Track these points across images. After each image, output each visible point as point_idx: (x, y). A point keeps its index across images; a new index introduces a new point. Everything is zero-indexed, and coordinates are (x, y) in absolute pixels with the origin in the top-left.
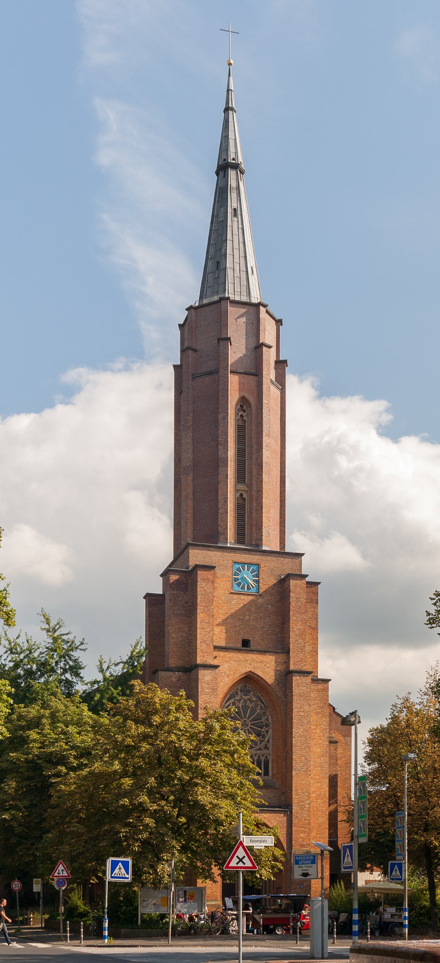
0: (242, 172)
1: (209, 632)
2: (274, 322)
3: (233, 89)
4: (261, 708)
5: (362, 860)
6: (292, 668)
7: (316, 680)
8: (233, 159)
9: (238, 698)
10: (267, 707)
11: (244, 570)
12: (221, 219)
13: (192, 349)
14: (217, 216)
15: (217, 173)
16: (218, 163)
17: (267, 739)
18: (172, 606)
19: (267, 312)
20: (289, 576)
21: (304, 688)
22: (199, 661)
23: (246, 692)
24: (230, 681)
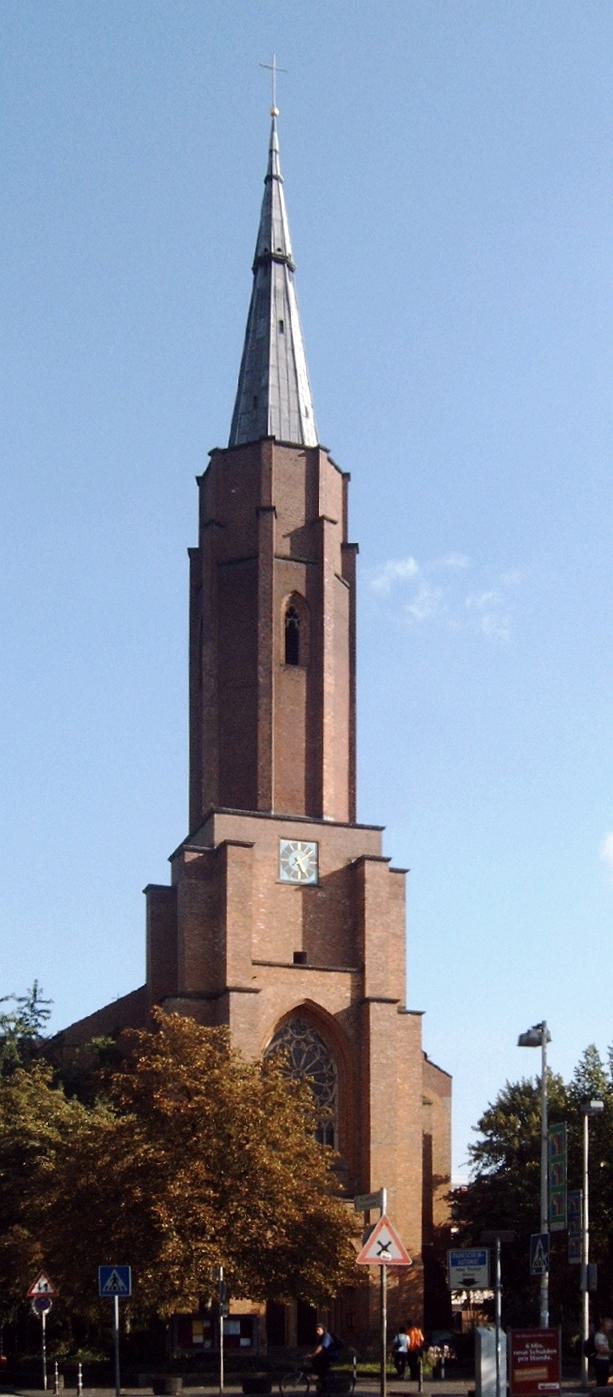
0: (291, 269)
1: (245, 940)
2: (340, 476)
3: (277, 149)
4: (322, 1053)
6: (368, 993)
7: (402, 1011)
8: (279, 250)
10: (333, 1051)
11: (296, 848)
12: (259, 336)
13: (218, 524)
14: (254, 331)
15: (255, 270)
16: (256, 255)
18: (187, 913)
19: (329, 460)
20: (361, 860)
21: (388, 1024)
22: (230, 982)
23: (300, 1030)
24: (277, 1014)
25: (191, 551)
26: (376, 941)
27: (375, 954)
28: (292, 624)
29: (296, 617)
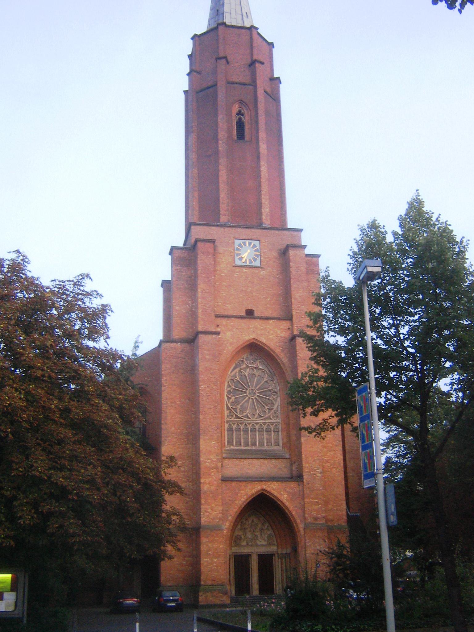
5: (48, 394)
9: (244, 366)
11: (245, 245)
17: (275, 408)
20: (287, 248)
25: (185, 92)
26: (299, 299)
27: (299, 307)
28: (240, 119)
29: (243, 115)
